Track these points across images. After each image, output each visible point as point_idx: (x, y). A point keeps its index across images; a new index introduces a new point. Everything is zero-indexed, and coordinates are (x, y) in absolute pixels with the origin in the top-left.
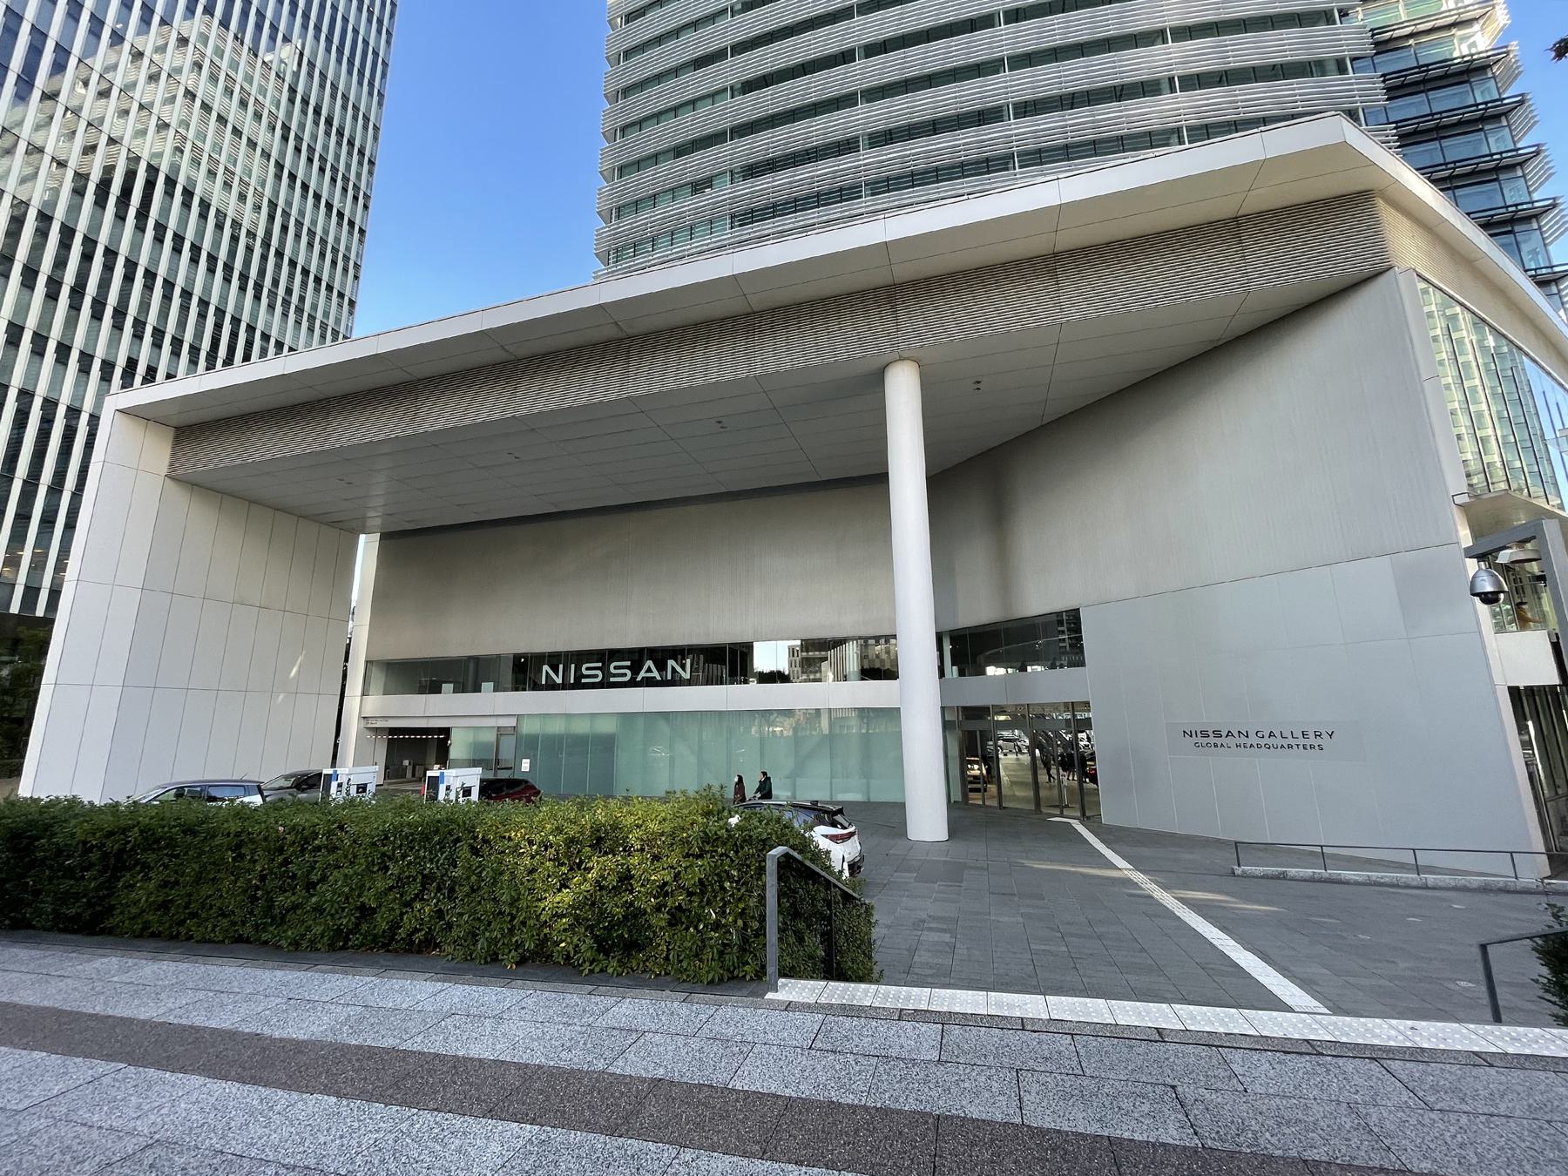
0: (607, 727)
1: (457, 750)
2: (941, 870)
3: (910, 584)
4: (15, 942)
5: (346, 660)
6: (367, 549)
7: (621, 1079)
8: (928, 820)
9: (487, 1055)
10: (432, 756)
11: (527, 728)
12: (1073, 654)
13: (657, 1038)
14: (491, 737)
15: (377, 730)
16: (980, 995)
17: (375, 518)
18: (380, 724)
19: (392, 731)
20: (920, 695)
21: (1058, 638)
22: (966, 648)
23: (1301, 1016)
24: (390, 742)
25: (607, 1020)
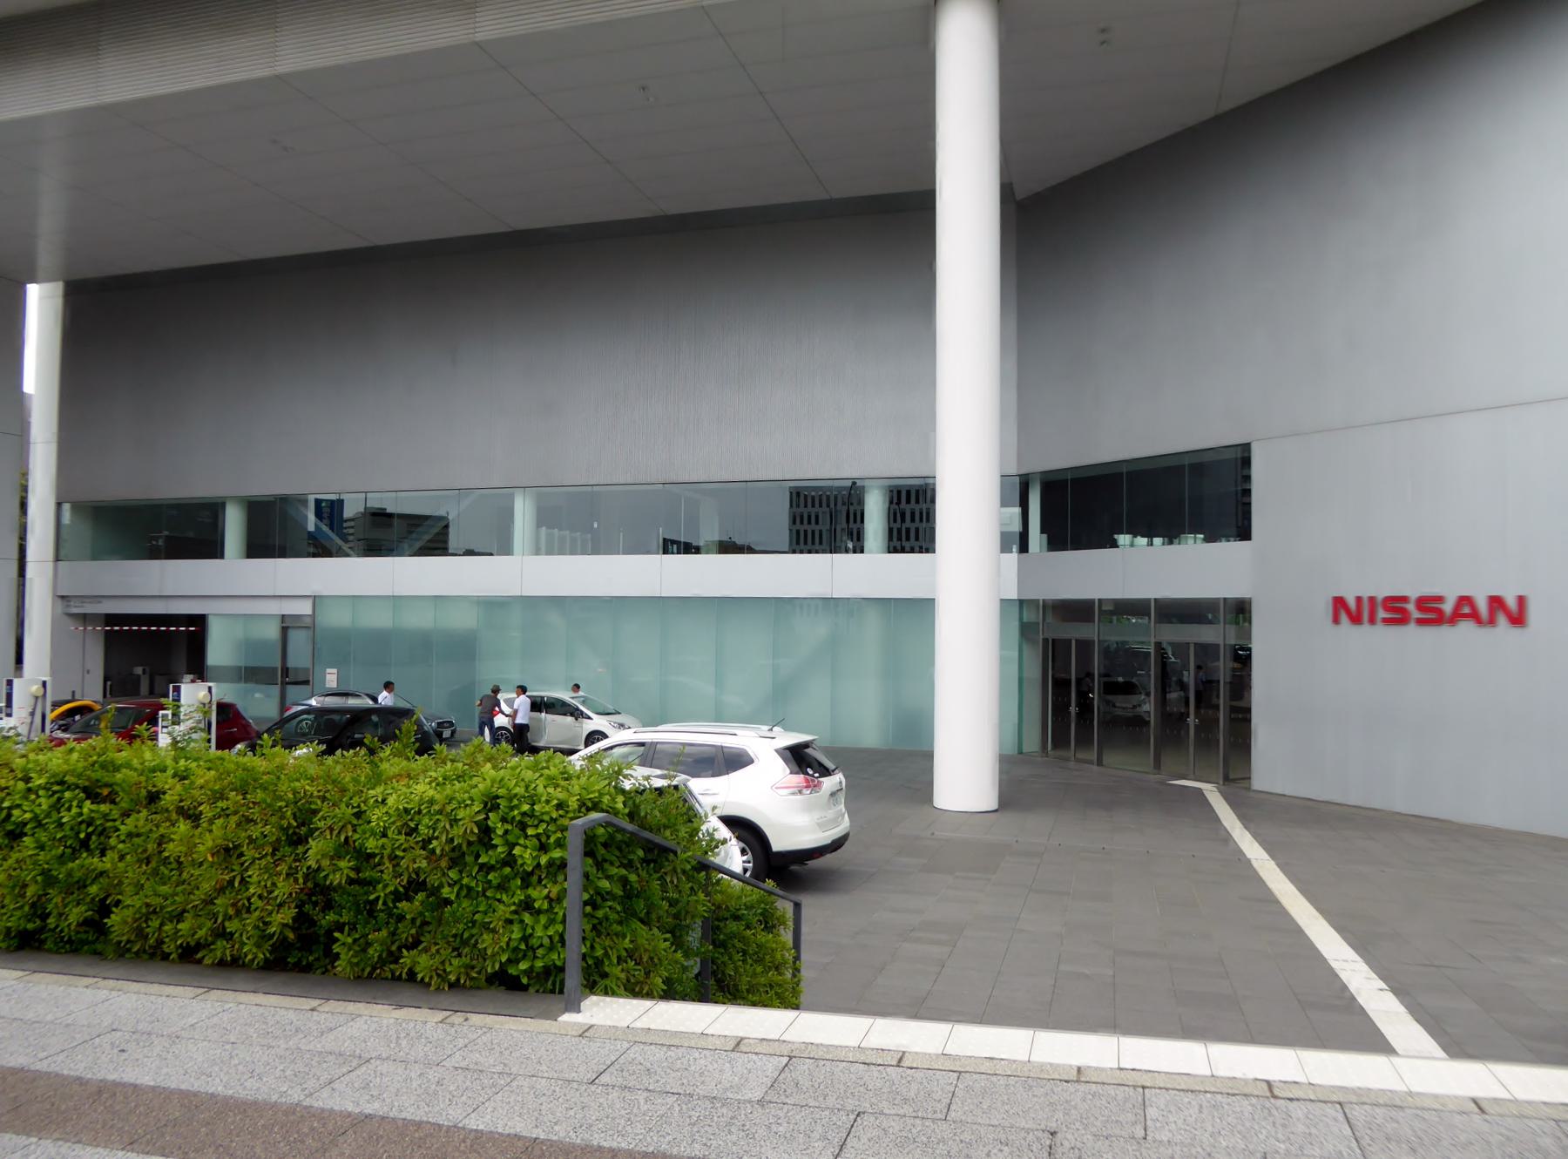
0: (463, 620)
1: (218, 652)
2: (965, 851)
3: (963, 394)
4: (373, 1000)
5: (1431, 612)
6: (40, 307)
7: (323, 1116)
8: (965, 776)
9: (147, 1080)
10: (181, 661)
11: (336, 618)
12: (1232, 520)
13: (384, 1068)
14: (272, 632)
15: (85, 618)
16: (862, 1022)
17: (47, 252)
18: (90, 609)
19: (111, 619)
20: (971, 577)
21: (1202, 494)
22: (1072, 505)
23: (1416, 1067)
24: (108, 636)
25: (328, 1043)
